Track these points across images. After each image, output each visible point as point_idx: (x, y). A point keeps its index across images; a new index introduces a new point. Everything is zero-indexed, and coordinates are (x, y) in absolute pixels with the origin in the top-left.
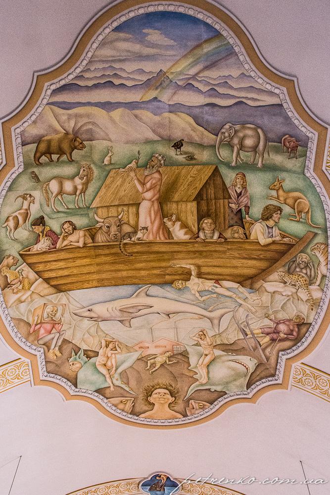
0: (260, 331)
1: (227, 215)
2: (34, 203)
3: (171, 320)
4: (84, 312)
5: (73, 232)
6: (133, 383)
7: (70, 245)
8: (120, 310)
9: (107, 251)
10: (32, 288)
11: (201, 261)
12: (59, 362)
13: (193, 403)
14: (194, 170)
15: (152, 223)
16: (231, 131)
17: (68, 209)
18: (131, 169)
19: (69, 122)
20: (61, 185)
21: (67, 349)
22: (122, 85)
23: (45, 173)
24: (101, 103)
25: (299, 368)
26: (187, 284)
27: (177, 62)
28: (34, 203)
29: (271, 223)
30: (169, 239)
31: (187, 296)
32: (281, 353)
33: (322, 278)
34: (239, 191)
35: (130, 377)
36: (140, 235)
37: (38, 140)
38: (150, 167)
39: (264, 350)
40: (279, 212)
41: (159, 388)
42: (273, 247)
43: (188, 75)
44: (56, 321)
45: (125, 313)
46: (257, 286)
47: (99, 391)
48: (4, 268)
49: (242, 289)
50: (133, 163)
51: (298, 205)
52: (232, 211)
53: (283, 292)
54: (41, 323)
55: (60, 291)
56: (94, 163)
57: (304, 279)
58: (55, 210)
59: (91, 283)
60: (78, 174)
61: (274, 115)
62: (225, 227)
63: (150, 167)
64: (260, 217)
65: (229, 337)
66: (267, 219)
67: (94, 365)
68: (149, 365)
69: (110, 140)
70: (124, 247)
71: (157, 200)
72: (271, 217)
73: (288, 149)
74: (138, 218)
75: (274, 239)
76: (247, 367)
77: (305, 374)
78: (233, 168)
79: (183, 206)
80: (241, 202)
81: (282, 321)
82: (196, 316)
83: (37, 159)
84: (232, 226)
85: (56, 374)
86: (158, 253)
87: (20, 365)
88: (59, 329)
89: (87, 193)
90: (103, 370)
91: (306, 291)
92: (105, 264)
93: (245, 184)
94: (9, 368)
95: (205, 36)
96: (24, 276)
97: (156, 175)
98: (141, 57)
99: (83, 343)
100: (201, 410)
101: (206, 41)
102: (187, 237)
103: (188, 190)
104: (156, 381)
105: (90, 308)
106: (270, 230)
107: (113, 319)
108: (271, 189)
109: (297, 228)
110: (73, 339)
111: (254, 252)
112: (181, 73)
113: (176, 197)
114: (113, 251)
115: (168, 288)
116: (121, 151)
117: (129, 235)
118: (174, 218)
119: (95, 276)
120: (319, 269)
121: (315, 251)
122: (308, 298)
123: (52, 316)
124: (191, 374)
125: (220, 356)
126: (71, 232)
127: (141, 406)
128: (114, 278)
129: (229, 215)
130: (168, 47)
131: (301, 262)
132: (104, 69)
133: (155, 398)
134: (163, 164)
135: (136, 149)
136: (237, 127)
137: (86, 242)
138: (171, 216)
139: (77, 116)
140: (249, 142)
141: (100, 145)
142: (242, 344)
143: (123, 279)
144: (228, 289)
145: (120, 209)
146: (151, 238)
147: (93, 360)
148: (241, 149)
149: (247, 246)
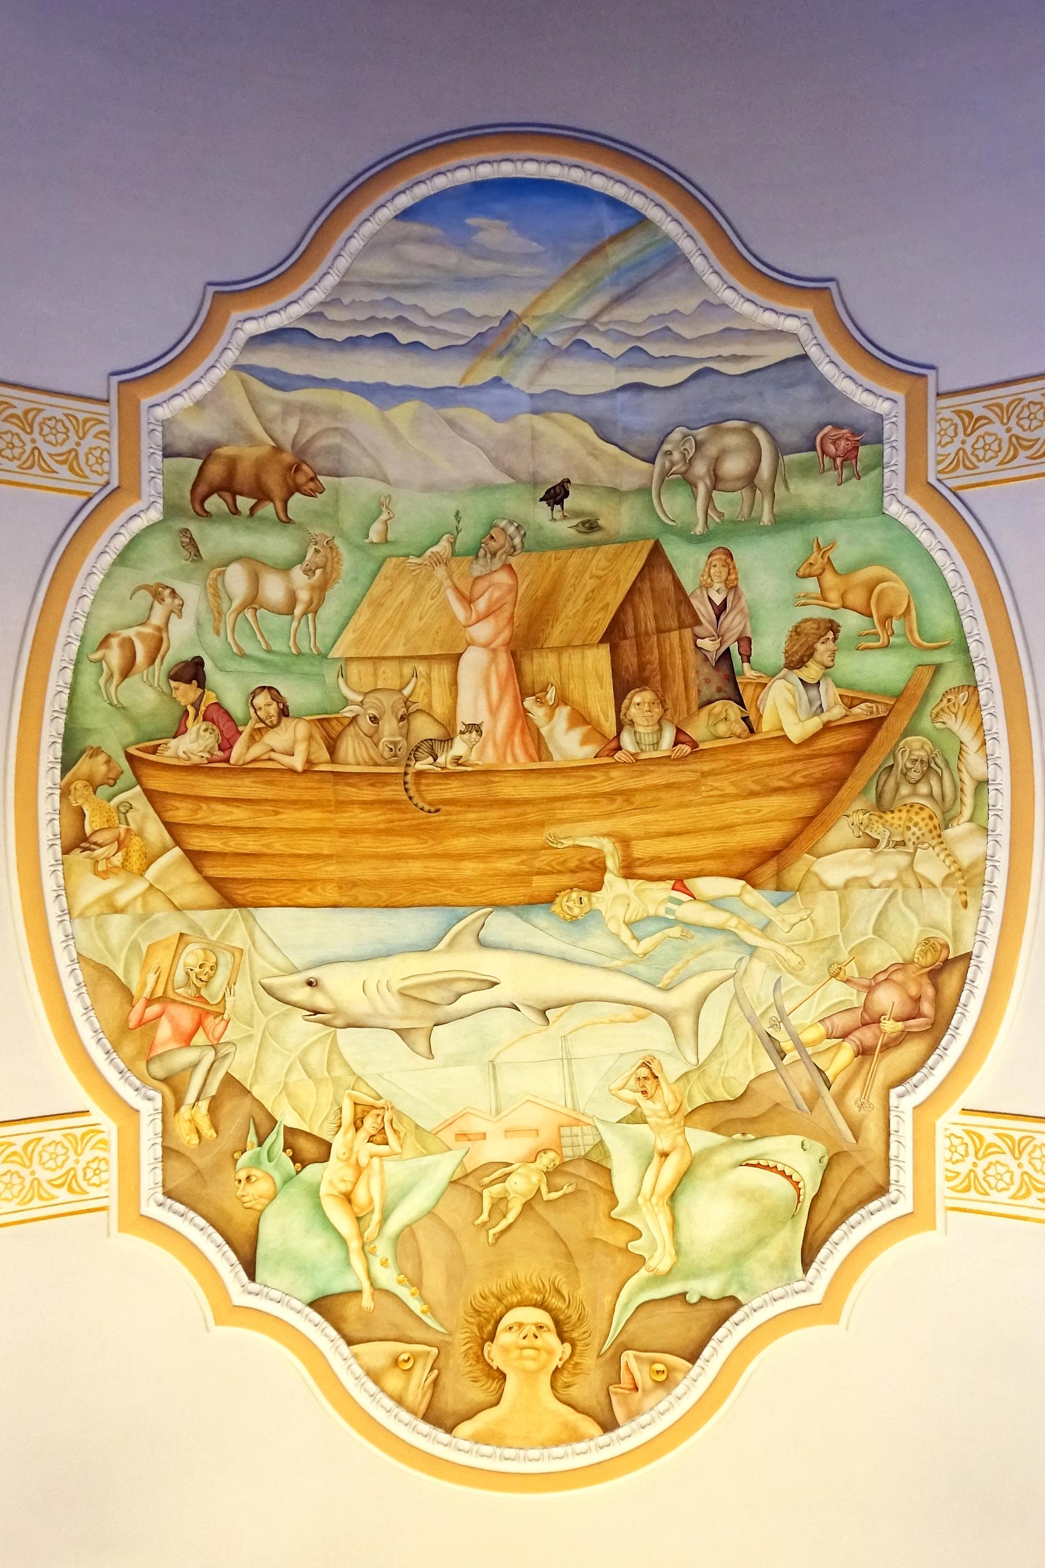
0: (821, 1030)
1: (692, 675)
2: (180, 616)
3: (552, 1028)
4: (293, 985)
5: (279, 722)
6: (435, 1279)
7: (270, 759)
8: (403, 994)
9: (369, 794)
10: (152, 873)
11: (634, 819)
12: (204, 1162)
13: (634, 1365)
14: (599, 560)
15: (494, 712)
16: (687, 446)
17: (269, 651)
18: (438, 560)
19: (284, 420)
20: (255, 581)
21: (235, 1114)
22: (416, 346)
23: (218, 538)
24: (363, 384)
25: (958, 1131)
26: (594, 900)
27: (546, 292)
28: (180, 616)
29: (811, 671)
30: (540, 760)
31: (597, 942)
32: (894, 1092)
33: (976, 789)
34: (718, 600)
35: (427, 1256)
36: (459, 747)
37: (206, 453)
38: (485, 555)
39: (840, 1100)
40: (830, 635)
41: (519, 1304)
42: (829, 741)
43: (576, 320)
44: (207, 1003)
45: (414, 1004)
46: (794, 874)
47: (320, 1304)
48: (79, 785)
49: (753, 896)
50: (444, 542)
51: (878, 601)
52: (706, 659)
53: (873, 875)
54: (164, 999)
55: (229, 902)
56: (343, 535)
57: (925, 814)
58: (235, 650)
59: (319, 889)
60: (301, 559)
61: (791, 385)
62: (689, 709)
63: (485, 555)
64: (783, 661)
65: (731, 1072)
66: (801, 663)
67: (314, 1192)
68: (487, 1205)
69: (385, 480)
70: (417, 784)
71: (507, 644)
72: (811, 655)
73: (835, 460)
74: (456, 696)
75: (826, 717)
76: (795, 1178)
77: (982, 1149)
78: (699, 540)
79: (573, 660)
80: (728, 630)
81: (882, 977)
82: (626, 1012)
83: (199, 496)
84: (709, 702)
85: (194, 1210)
86: (508, 803)
87: (86, 1133)
88: (217, 1034)
89: (323, 613)
90: (342, 1220)
91: (937, 849)
92: (363, 831)
93: (733, 577)
94: (48, 1137)
95: (611, 227)
96: (133, 826)
97: (503, 578)
98: (461, 282)
99: (284, 1101)
100: (660, 1393)
101: (614, 239)
102: (590, 750)
103: (586, 611)
104: (508, 1275)
105: (312, 974)
106: (813, 692)
107: (379, 1021)
108: (804, 577)
109: (883, 669)
110: (255, 1080)
111: (775, 770)
112: (557, 317)
113: (556, 635)
114: (390, 792)
115: (540, 917)
116: (415, 514)
117: (432, 747)
118: (551, 694)
119: (333, 870)
120: (963, 769)
121: (945, 718)
122: (947, 871)
123: (199, 984)
124: (618, 1238)
125: (709, 1152)
126: (275, 720)
127: (462, 1388)
128: (382, 883)
129: (697, 672)
130: (529, 258)
131: (909, 765)
132: (374, 303)
133: (505, 1350)
134: (519, 547)
135: (450, 505)
136: (702, 433)
137: (313, 757)
138: (545, 690)
139: (305, 409)
140: (734, 466)
141: (357, 492)
142: (774, 1091)
143: (410, 883)
144: (714, 903)
145: (407, 670)
146: (490, 758)
147: (312, 1171)
148: (714, 489)
149: (757, 757)
